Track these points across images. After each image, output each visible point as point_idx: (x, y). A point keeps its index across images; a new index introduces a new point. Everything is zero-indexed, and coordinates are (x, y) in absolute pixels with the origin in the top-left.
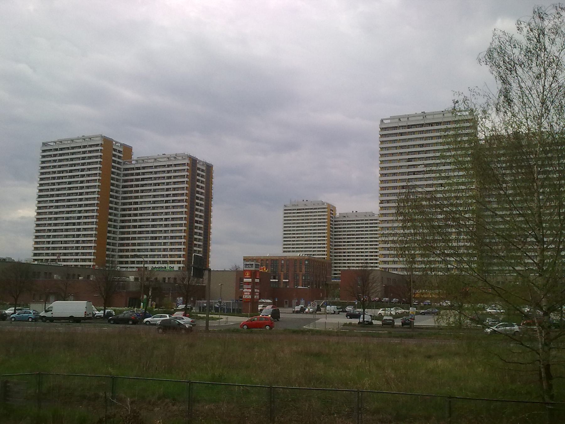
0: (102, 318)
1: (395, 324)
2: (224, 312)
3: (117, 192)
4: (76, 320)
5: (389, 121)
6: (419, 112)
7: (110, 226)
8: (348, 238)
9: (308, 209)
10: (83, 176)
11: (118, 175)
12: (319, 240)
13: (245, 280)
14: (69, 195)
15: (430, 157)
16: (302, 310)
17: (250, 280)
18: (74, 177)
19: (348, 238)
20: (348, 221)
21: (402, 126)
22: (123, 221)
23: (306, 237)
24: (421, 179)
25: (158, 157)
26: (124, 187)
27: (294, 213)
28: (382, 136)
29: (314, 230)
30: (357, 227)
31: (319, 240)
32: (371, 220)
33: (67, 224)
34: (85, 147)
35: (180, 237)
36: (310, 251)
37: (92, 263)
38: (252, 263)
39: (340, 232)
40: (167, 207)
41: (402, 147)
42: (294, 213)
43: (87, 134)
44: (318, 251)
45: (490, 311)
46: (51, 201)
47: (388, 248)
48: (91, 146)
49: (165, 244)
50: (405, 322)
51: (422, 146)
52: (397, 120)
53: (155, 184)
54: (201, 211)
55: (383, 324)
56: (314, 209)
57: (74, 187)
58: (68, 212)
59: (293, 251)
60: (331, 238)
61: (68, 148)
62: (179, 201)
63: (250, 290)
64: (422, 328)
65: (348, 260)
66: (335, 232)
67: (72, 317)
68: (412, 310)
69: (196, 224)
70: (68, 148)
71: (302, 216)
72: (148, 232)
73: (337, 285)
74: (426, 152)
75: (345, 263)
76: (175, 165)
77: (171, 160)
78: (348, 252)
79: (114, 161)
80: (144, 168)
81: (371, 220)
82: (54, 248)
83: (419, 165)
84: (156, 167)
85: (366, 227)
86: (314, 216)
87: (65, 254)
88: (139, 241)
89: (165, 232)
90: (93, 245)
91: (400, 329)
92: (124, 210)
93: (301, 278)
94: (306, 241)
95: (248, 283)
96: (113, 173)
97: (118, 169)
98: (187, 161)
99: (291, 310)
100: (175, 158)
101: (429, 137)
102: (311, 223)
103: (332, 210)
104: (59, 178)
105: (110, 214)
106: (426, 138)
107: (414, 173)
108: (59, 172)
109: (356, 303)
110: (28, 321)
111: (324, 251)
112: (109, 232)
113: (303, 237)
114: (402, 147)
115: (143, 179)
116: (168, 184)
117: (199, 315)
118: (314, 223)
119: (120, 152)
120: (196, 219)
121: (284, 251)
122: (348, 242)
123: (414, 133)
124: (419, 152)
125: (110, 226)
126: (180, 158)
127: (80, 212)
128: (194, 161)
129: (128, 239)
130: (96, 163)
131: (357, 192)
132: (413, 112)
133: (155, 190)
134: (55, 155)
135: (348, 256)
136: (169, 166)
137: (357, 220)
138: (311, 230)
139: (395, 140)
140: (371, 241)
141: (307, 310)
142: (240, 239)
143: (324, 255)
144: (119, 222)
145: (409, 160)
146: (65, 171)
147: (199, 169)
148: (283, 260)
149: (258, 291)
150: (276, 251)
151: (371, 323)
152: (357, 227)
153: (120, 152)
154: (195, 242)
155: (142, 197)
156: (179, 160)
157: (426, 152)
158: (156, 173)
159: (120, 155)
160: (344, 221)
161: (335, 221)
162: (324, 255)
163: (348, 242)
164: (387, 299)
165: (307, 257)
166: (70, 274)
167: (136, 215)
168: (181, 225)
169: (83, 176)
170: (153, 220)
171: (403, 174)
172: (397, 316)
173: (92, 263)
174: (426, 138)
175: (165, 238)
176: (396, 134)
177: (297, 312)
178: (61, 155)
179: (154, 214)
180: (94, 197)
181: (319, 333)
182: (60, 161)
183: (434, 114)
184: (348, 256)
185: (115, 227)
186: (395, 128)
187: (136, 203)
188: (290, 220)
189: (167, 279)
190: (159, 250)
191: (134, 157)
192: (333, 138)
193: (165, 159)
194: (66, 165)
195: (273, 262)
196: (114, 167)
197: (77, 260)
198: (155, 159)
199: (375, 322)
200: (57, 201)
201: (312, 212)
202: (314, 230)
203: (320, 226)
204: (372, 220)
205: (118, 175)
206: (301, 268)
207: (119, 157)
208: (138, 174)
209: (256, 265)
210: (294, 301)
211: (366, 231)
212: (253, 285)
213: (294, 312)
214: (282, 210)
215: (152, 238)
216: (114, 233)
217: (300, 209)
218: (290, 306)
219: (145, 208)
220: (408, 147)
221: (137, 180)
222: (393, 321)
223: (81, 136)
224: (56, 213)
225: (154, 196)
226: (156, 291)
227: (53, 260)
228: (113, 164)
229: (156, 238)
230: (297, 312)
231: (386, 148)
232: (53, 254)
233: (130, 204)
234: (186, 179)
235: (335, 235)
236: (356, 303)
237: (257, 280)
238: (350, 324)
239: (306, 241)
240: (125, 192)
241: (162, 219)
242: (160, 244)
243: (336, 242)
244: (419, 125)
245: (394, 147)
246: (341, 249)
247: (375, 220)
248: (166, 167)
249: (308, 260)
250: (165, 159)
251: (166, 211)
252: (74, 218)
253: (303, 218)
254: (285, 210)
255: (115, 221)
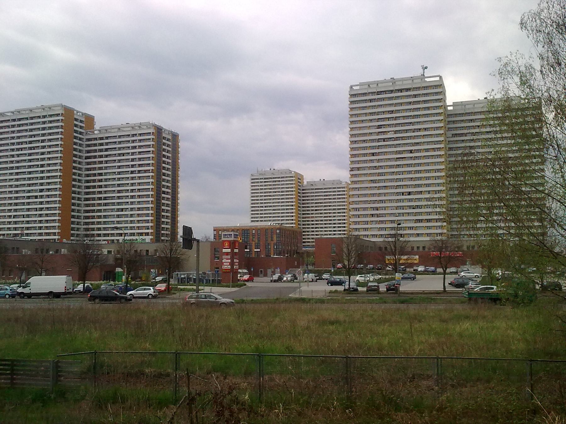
0: (82, 292)
1: (380, 290)
2: (203, 283)
3: (80, 163)
4: (57, 295)
5: (358, 88)
6: (388, 78)
7: (74, 198)
8: (316, 207)
9: (276, 178)
10: (44, 147)
11: (81, 145)
12: (287, 209)
13: (224, 250)
14: (30, 167)
15: (399, 124)
16: (280, 279)
17: (229, 250)
18: (34, 148)
19: (316, 207)
20: (316, 189)
21: (372, 93)
22: (87, 193)
23: (274, 206)
24: (390, 146)
25: (122, 126)
26: (87, 158)
27: (261, 182)
28: (352, 102)
29: (282, 199)
30: (325, 196)
31: (287, 209)
32: (338, 188)
33: (29, 197)
34: (44, 117)
35: (147, 209)
36: (279, 220)
37: (56, 237)
38: (230, 233)
39: (308, 200)
40: (133, 178)
41: (371, 114)
42: (261, 182)
43: (46, 104)
44: (287, 220)
45: (464, 274)
46: (11, 174)
47: (437, 219)
48: (51, 116)
49: (132, 216)
50: (389, 287)
51: (392, 112)
52: (367, 86)
53: (120, 155)
54: (168, 181)
55: (367, 291)
56: (282, 178)
57: (34, 159)
58: (29, 185)
59: (261, 221)
60: (299, 207)
61: (27, 119)
62: (145, 171)
63: (230, 261)
64: (408, 293)
65: (316, 228)
66: (303, 200)
67: (51, 292)
68: (398, 276)
69: (163, 195)
70: (27, 119)
71: (270, 185)
72: (113, 204)
73: (308, 254)
74: (396, 118)
75: (313, 231)
76: (140, 135)
77: (136, 129)
78: (317, 221)
79: (76, 132)
80: (107, 138)
81: (338, 188)
82: (16, 223)
83: (389, 132)
84: (120, 137)
85: (334, 195)
86: (282, 184)
87: (28, 228)
88: (105, 214)
89: (132, 203)
90: (57, 218)
91: (385, 295)
92: (88, 181)
93: (272, 247)
94: (274, 210)
95: (227, 254)
96: (75, 144)
97: (80, 139)
98: (151, 131)
99: (268, 279)
100: (140, 127)
101: (399, 103)
102: (279, 192)
103: (299, 178)
104: (18, 150)
105: (74, 186)
106: (396, 105)
107: (384, 140)
108: (18, 143)
109: (333, 271)
110: (5, 297)
111: (293, 220)
112: (74, 204)
113: (271, 206)
114: (371, 114)
115: (106, 150)
116: (133, 154)
117: (179, 287)
118: (282, 192)
119: (81, 121)
120: (163, 189)
121: (252, 221)
122: (316, 210)
123: (383, 99)
124: (389, 119)
125: (74, 198)
126: (145, 127)
127: (42, 184)
128: (159, 130)
129: (93, 211)
130: (57, 133)
131: (323, 158)
132: (382, 79)
133: (119, 161)
134: (13, 126)
135: (317, 224)
136: (134, 135)
137: (325, 189)
138: (279, 199)
139: (364, 107)
140: (338, 209)
141: (285, 279)
142: (211, 208)
143: (293, 223)
144: (83, 193)
145: (379, 127)
146: (25, 142)
147: (164, 138)
148: (253, 229)
149: (238, 261)
150: (244, 221)
151: (357, 290)
152: (325, 196)
153: (81, 121)
154: (163, 214)
155: (106, 168)
156: (143, 129)
157: (396, 118)
158: (120, 143)
159: (82, 125)
160: (312, 189)
161: (303, 190)
162: (293, 223)
163: (316, 210)
164: (362, 265)
165: (278, 226)
166: (41, 248)
167: (100, 187)
168: (148, 196)
169: (44, 147)
170: (119, 192)
171: (373, 141)
172: (379, 281)
173: (56, 237)
174: (396, 105)
175: (132, 209)
176: (365, 101)
177: (275, 281)
178: (19, 126)
179: (119, 185)
180: (57, 169)
181: (303, 300)
182: (19, 131)
183: (403, 80)
184: (317, 224)
185: (79, 199)
186: (365, 94)
187: (100, 174)
188: (258, 189)
189: (415, 249)
190: (126, 222)
191: (97, 126)
192: (286, 101)
193: (130, 129)
194: (26, 136)
195: (245, 232)
196: (76, 138)
197: (40, 234)
198: (119, 129)
199: (360, 289)
200: (17, 174)
201: (279, 181)
202: (282, 199)
203: (340, 198)
204: (340, 188)
205: (81, 145)
206: (272, 238)
207: (81, 127)
208: (101, 144)
209: (235, 235)
210: (269, 271)
211: (334, 199)
212: (233, 255)
213: (271, 281)
214: (249, 179)
215: (118, 210)
216: (79, 205)
217: (267, 178)
218: (266, 275)
219: (110, 179)
220: (378, 113)
221: (101, 150)
222: (378, 286)
223: (39, 105)
224: (17, 186)
225: (119, 167)
226: (134, 263)
227: (16, 235)
228: (75, 134)
229: (122, 210)
230: (275, 281)
231: (355, 115)
232: (15, 229)
233: (95, 175)
234: (151, 149)
235: (303, 204)
236: (333, 271)
237: (236, 251)
238: (336, 291)
239: (274, 210)
240: (88, 164)
241: (128, 190)
242: (126, 216)
243: (304, 211)
244: (388, 91)
245: (364, 114)
246: (309, 217)
247: (343, 188)
248: (130, 136)
249: (279, 229)
250: (130, 129)
251: (132, 182)
252: (36, 191)
253: (270, 187)
254: (253, 179)
255: (79, 193)
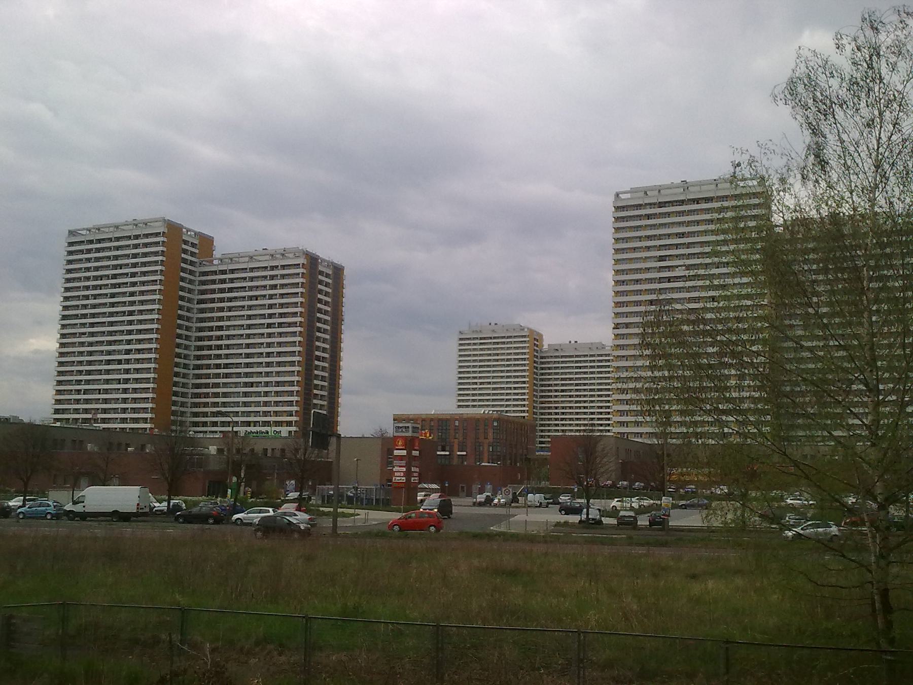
0: (165, 513)
1: (639, 523)
2: (362, 504)
3: (189, 310)
4: (123, 517)
5: (628, 196)
6: (678, 181)
7: (177, 365)
8: (563, 385)
9: (498, 338)
10: (134, 284)
11: (191, 282)
12: (515, 388)
13: (396, 453)
14: (112, 314)
15: (694, 254)
16: (488, 502)
17: (404, 453)
18: (119, 285)
19: (563, 385)
20: (562, 357)
21: (650, 204)
22: (198, 358)
23: (494, 383)
24: (680, 289)
25: (256, 253)
26: (200, 302)
27: (475, 344)
28: (617, 219)
29: (508, 371)
30: (577, 367)
31: (515, 388)
32: (599, 355)
33: (109, 362)
34: (137, 237)
35: (291, 383)
36: (501, 406)
37: (148, 426)
38: (407, 425)
39: (549, 374)
40: (270, 335)
41: (649, 238)
42: (475, 344)
43: (141, 216)
44: (515, 406)
45: (792, 502)
46: (83, 325)
47: (627, 401)
48: (147, 236)
49: (266, 394)
50: (654, 520)
51: (682, 235)
52: (642, 194)
53: (251, 298)
54: (325, 341)
55: (619, 524)
56: (508, 337)
57: (119, 303)
58: (110, 343)
59: (474, 406)
60: (535, 385)
61: (110, 240)
62: (290, 325)
63: (404, 469)
64: (682, 531)
65: (562, 419)
66: (542, 374)
67: (116, 512)
68: (666, 501)
69: (317, 363)
70: (110, 240)
71: (489, 349)
72: (238, 375)
73: (544, 461)
74: (689, 246)
75: (557, 425)
76: (283, 267)
77: (276, 259)
78: (563, 408)
79: (185, 261)
80: (232, 271)
81: (599, 355)
82: (87, 401)
83: (677, 267)
84: (252, 270)
85: (592, 367)
86: (508, 348)
87: (105, 411)
88: (225, 390)
89: (267, 374)
90: (150, 395)
91: (646, 532)
92: (200, 339)
93: (486, 449)
94: (494, 389)
95: (401, 458)
96: (183, 279)
97: (191, 273)
98: (301, 261)
99: (470, 500)
100: (283, 255)
101: (694, 222)
102: (502, 360)
103: (536, 339)
104: (95, 287)
105: (178, 346)
106: (689, 223)
107: (669, 280)
108: (96, 278)
109: (576, 490)
110: (45, 518)
111: (524, 405)
112: (177, 375)
113: (489, 383)
114: (649, 238)
115: (231, 290)
116: (271, 297)
117: (321, 509)
118: (508, 360)
119: (193, 245)
120: (317, 353)
121: (459, 406)
122: (563, 391)
123: (668, 214)
124: (677, 246)
125: (177, 365)
126: (291, 255)
127: (129, 342)
128: (313, 261)
129: (207, 386)
130: (156, 263)
131: (578, 310)
132: (667, 182)
133: (250, 308)
134: (89, 251)
135: (563, 413)
136: (273, 268)
137: (577, 356)
138: (502, 371)
139: (638, 227)
140: (599, 390)
141: (496, 501)
142: (387, 386)
143: (524, 411)
144: (192, 358)
145: (662, 258)
146: (105, 276)
147: (321, 273)
148: (457, 419)
149: (417, 470)
150: (445, 405)
151: (600, 522)
152: (577, 367)
153: (193, 245)
154: (315, 392)
155: (229, 318)
156: (289, 258)
157: (689, 246)
158: (252, 279)
159: (193, 250)
160: (556, 357)
161: (542, 358)
162: (524, 411)
163: (563, 391)
164: (625, 483)
165: (495, 415)
166: (113, 442)
167: (219, 347)
168: (292, 363)
169: (134, 284)
170: (248, 356)
171: (651, 281)
172: (641, 511)
173: (148, 426)
174: (689, 223)
175: (267, 384)
176: (640, 217)
177: (480, 504)
178: (98, 250)
179: (248, 346)
180: (152, 318)
181: (515, 537)
182: (97, 259)
183: (701, 184)
184: (563, 413)
185: (186, 366)
186: (639, 207)
187: (220, 328)
188: (469, 355)
189: (269, 451)
190: (258, 404)
191: (217, 254)
193: (267, 257)
194: (107, 267)
195: (441, 423)
196: (184, 270)
197: (124, 420)
198: (251, 257)
199: (606, 520)
200: (92, 325)
201: (504, 343)
202: (508, 371)
203: (518, 365)
204: (601, 355)
205: (191, 282)
206: (486, 433)
207: (193, 254)
208: (223, 281)
209: (413, 427)
210: (476, 487)
211: (592, 373)
212: (409, 460)
213: (474, 504)
214: (456, 338)
215: (246, 385)
216: (185, 376)
217: (484, 338)
218: (469, 494)
219: (234, 336)
220: (660, 237)
221: (222, 291)
222: (635, 518)
223: (130, 219)
224: (91, 344)
225: (249, 317)
226: (252, 470)
227: (85, 421)
228: (183, 265)
229: (252, 385)
230: (480, 504)
231: (623, 239)
232: (86, 411)
233: (211, 329)
234: (300, 290)
235: (542, 380)
236: (576, 490)
237: (415, 453)
238: (566, 523)
239: (494, 389)
240: (202, 311)
241: (262, 354)
242: (258, 394)
243: (542, 391)
244: (676, 201)
245: (637, 237)
246: (550, 402)
247: (606, 355)
248: (268, 269)
249: (498, 420)
250: (267, 257)
251: (269, 340)
252: (119, 352)
253: (489, 352)
254: (461, 339)
255: (186, 357)
